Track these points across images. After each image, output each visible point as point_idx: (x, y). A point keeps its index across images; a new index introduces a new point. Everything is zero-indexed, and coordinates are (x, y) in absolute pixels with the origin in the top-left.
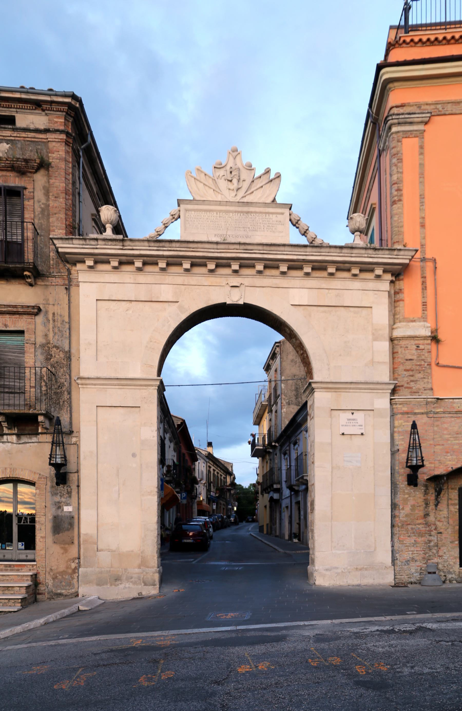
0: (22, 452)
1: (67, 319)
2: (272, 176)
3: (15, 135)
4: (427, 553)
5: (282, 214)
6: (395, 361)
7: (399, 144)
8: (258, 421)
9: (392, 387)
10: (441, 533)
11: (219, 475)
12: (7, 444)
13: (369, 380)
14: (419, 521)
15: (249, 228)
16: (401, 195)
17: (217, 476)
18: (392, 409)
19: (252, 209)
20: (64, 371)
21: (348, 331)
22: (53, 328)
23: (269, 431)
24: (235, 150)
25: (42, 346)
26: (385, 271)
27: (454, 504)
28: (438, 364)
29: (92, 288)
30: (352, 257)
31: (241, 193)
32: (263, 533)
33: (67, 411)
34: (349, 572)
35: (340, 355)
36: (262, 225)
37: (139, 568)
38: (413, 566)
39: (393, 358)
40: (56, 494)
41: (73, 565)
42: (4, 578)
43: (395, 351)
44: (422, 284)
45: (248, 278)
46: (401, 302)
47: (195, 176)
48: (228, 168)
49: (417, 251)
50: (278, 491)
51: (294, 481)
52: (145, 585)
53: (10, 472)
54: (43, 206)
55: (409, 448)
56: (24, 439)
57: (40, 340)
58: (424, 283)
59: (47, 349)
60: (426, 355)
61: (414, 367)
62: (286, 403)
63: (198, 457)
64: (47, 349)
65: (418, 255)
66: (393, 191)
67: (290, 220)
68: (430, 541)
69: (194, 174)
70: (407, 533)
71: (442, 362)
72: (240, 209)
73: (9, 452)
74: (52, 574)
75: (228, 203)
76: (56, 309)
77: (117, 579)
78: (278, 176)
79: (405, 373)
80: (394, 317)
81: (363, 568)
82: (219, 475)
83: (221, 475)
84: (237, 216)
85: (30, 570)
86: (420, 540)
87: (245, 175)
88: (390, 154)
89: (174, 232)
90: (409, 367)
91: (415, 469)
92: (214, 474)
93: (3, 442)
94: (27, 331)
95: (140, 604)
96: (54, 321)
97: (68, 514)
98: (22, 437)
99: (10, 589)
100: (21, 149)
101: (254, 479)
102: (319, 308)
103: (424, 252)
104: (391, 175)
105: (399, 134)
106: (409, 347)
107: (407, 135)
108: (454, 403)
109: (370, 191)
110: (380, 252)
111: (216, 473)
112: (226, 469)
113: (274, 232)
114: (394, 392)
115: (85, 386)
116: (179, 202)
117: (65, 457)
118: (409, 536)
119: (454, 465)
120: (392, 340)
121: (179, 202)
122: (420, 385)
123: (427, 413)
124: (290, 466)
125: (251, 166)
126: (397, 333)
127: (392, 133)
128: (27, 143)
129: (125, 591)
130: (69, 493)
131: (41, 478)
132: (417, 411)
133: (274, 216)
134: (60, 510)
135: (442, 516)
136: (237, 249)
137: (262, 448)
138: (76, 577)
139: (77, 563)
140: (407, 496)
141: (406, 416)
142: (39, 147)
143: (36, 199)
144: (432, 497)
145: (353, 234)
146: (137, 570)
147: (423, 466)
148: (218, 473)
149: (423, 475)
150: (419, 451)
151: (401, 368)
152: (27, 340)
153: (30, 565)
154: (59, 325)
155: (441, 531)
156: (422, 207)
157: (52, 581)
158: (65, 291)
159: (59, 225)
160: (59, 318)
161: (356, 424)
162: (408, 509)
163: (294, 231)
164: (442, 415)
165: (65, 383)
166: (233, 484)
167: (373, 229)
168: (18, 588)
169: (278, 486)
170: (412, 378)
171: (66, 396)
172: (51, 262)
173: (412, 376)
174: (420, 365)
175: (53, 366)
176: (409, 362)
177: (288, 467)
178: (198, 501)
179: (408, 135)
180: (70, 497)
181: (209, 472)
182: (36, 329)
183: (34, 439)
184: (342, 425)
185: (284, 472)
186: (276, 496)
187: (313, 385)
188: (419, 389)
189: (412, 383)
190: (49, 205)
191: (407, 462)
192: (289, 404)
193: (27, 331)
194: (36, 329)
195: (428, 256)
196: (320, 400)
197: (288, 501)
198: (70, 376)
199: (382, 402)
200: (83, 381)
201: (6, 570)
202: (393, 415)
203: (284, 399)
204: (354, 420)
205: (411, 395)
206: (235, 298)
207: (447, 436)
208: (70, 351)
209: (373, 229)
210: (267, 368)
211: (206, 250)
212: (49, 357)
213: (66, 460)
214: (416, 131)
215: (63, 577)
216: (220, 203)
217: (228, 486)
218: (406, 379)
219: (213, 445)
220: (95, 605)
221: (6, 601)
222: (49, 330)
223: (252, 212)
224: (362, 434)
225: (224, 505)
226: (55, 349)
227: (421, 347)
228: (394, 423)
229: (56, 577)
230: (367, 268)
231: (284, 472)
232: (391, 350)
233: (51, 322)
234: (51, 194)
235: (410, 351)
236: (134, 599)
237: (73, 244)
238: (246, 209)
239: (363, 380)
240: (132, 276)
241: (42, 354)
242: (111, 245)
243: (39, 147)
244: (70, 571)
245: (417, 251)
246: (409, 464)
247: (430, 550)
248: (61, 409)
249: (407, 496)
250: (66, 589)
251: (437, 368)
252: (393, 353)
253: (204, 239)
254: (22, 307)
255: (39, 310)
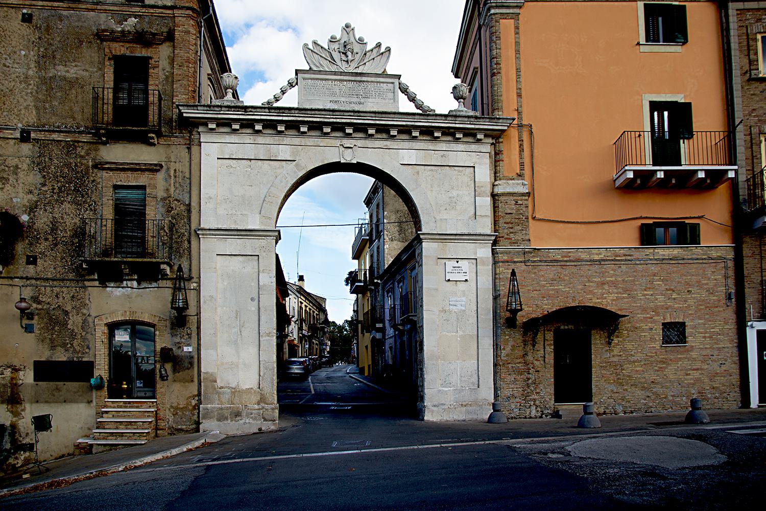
0: (142, 296)
1: (187, 175)
2: (383, 49)
3: (143, 11)
4: (525, 390)
5: (393, 83)
6: (496, 214)
7: (498, 24)
8: (357, 255)
9: (493, 238)
10: (538, 371)
11: (311, 312)
12: (127, 289)
13: (472, 232)
14: (519, 361)
15: (362, 95)
16: (500, 69)
17: (310, 313)
18: (494, 258)
19: (364, 79)
20: (184, 222)
21: (452, 190)
22: (174, 183)
23: (371, 267)
24: (347, 26)
25: (164, 199)
26: (486, 136)
27: (550, 345)
28: (534, 218)
29: (213, 149)
30: (456, 123)
31: (353, 65)
32: (364, 375)
33: (187, 258)
34: (455, 408)
35: (446, 209)
36: (374, 93)
37: (258, 404)
38: (513, 402)
39: (495, 212)
40: (176, 335)
41: (194, 402)
42: (125, 414)
43: (496, 205)
44: (520, 147)
45: (358, 142)
46: (501, 162)
47: (312, 48)
48: (342, 42)
49: (514, 119)
50: (382, 330)
51: (398, 319)
52: (265, 420)
53: (130, 315)
54: (167, 74)
55: (509, 294)
56: (144, 285)
57: (161, 194)
58: (521, 146)
59: (167, 203)
60: (524, 209)
61: (513, 220)
62: (389, 239)
63: (289, 292)
64: (167, 203)
65: (515, 122)
66: (493, 64)
67: (400, 88)
68: (529, 379)
69: (311, 47)
70: (508, 372)
71: (538, 216)
72: (353, 78)
73: (129, 297)
74: (172, 410)
75: (341, 73)
76: (178, 166)
77: (237, 414)
78: (388, 50)
79: (505, 225)
80: (496, 175)
81: (468, 404)
82: (311, 312)
83: (314, 312)
84: (350, 85)
85: (150, 407)
86: (518, 378)
87: (357, 48)
88: (490, 31)
89: (291, 100)
90: (508, 219)
91: (514, 312)
92: (305, 310)
93: (122, 287)
94: (149, 186)
95: (261, 439)
96: (175, 177)
97: (188, 354)
98: (142, 283)
99: (133, 424)
100: (149, 23)
101: (348, 315)
102: (426, 167)
103: (520, 118)
104: (491, 50)
105: (496, 16)
106: (509, 202)
107: (504, 17)
108: (549, 252)
109: (472, 54)
110: (481, 120)
111: (308, 309)
112: (318, 304)
113: (384, 99)
114: (495, 243)
115: (205, 236)
116: (297, 72)
117: (186, 302)
118: (510, 375)
119: (550, 309)
120: (494, 196)
121: (297, 72)
122: (519, 237)
123: (525, 262)
124: (395, 305)
125: (363, 41)
126: (498, 190)
127: (491, 14)
128: (154, 18)
129: (247, 425)
130: (190, 335)
131: (161, 320)
132: (516, 260)
133: (385, 84)
134: (180, 350)
135: (539, 355)
136: (351, 116)
137: (363, 284)
138: (196, 414)
139: (198, 400)
140: (507, 337)
141: (507, 264)
142: (166, 21)
143: (161, 67)
144: (529, 338)
145: (457, 100)
146: (256, 407)
147: (521, 310)
148: (310, 309)
149: (521, 318)
150: (517, 296)
151: (501, 221)
152: (149, 194)
153: (150, 402)
154: (180, 181)
155: (539, 369)
156: (518, 80)
157: (173, 417)
158: (187, 151)
159: (183, 90)
160: (181, 174)
161: (461, 271)
162: (508, 349)
163: (402, 98)
164: (539, 264)
165: (186, 233)
166: (326, 321)
167: (476, 90)
168: (141, 423)
169: (381, 325)
170: (511, 230)
171: (186, 244)
172: (174, 124)
173: (512, 228)
174: (519, 219)
175: (173, 218)
176: (509, 216)
177: (392, 306)
178: (289, 341)
179: (504, 16)
180: (190, 338)
181: (301, 308)
182: (158, 185)
183: (154, 285)
184: (448, 273)
185: (387, 311)
186: (379, 336)
187: (421, 237)
188: (519, 240)
189: (511, 235)
190: (173, 73)
191: (507, 306)
192: (392, 240)
193: (149, 186)
194: (158, 185)
195: (525, 122)
196: (428, 248)
197: (392, 340)
198: (190, 227)
199: (484, 252)
200: (204, 232)
201: (126, 407)
202: (495, 263)
203: (387, 235)
204: (459, 267)
205: (511, 246)
206: (348, 157)
207: (543, 283)
208: (190, 204)
209: (476, 90)
210: (368, 202)
211: (323, 116)
212: (169, 209)
213: (187, 304)
214: (512, 13)
215: (183, 414)
216: (335, 73)
217: (321, 324)
218: (506, 231)
219: (304, 278)
220: (220, 439)
221: (131, 435)
222: (170, 185)
223: (364, 81)
224: (466, 280)
225: (317, 344)
226: (176, 202)
227: (520, 202)
228: (495, 271)
229: (177, 413)
230: (470, 134)
231: (387, 311)
232: (492, 205)
233: (173, 178)
234: (175, 63)
235: (508, 206)
236: (254, 433)
237: (198, 110)
238: (358, 78)
239: (466, 232)
240: (252, 137)
241: (163, 206)
242: (234, 111)
243: (166, 21)
244: (190, 408)
245: (514, 119)
246: (509, 308)
247: (528, 387)
248: (181, 257)
249: (507, 337)
250: (186, 425)
251: (534, 222)
252: (495, 208)
253: (321, 107)
254: (145, 164)
255: (161, 166)
